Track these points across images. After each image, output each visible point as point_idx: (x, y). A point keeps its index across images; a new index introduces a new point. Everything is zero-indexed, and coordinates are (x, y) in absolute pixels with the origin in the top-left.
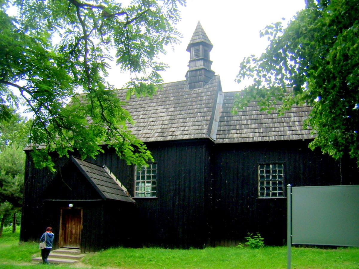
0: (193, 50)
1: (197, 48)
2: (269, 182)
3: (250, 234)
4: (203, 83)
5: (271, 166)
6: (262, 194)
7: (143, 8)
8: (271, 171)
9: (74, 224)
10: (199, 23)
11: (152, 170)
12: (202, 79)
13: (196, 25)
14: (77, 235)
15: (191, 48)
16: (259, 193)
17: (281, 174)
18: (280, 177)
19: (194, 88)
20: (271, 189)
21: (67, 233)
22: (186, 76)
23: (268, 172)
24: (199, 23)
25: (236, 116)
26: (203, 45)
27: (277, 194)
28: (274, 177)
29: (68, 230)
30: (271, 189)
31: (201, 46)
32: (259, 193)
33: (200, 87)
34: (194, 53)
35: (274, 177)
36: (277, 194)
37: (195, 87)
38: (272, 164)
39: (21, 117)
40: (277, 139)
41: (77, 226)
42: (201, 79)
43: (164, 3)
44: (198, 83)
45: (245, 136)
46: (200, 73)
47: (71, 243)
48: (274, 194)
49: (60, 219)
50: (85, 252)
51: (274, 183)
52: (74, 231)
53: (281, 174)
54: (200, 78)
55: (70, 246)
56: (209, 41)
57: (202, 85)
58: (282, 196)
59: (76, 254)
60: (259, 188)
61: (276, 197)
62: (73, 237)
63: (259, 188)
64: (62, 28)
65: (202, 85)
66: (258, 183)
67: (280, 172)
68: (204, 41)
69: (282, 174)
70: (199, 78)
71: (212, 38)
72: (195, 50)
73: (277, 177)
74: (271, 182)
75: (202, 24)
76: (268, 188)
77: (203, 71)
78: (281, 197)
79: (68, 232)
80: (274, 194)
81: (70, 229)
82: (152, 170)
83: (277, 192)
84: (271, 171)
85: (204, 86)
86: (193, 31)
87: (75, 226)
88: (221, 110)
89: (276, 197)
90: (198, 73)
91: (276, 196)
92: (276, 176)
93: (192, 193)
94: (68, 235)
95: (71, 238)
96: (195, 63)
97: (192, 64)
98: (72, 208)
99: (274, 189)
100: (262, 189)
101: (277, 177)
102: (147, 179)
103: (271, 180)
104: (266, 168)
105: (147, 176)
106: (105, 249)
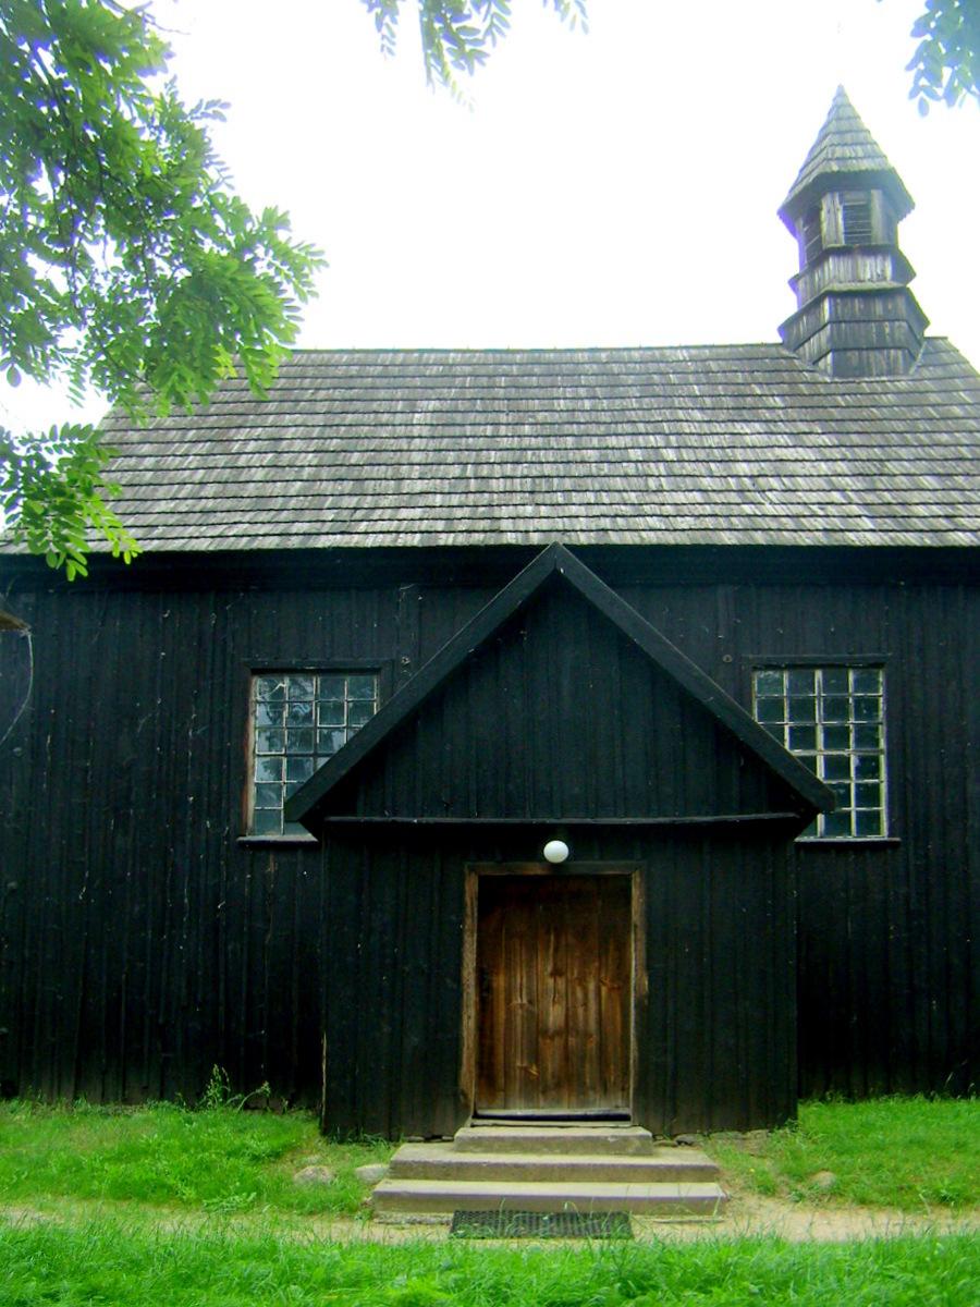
0: (841, 208)
9: (556, 973)
10: (841, 93)
11: (858, 701)
12: (897, 335)
13: (833, 93)
14: (587, 1035)
19: (862, 375)
21: (501, 1029)
22: (785, 329)
24: (841, 93)
29: (509, 1012)
34: (841, 221)
37: (863, 370)
39: (211, 153)
41: (582, 980)
43: (282, 235)
44: (877, 353)
47: (535, 1088)
49: (460, 944)
50: (672, 1137)
52: (554, 1015)
54: (887, 330)
55: (530, 1100)
59: (620, 1146)
62: (552, 1053)
72: (845, 208)
79: (509, 1021)
81: (520, 1000)
82: (858, 701)
87: (561, 982)
90: (878, 308)
93: (200, 949)
94: (522, 1051)
95: (536, 1056)
96: (855, 268)
98: (556, 867)
102: (827, 745)
105: (828, 731)
106: (850, 1098)
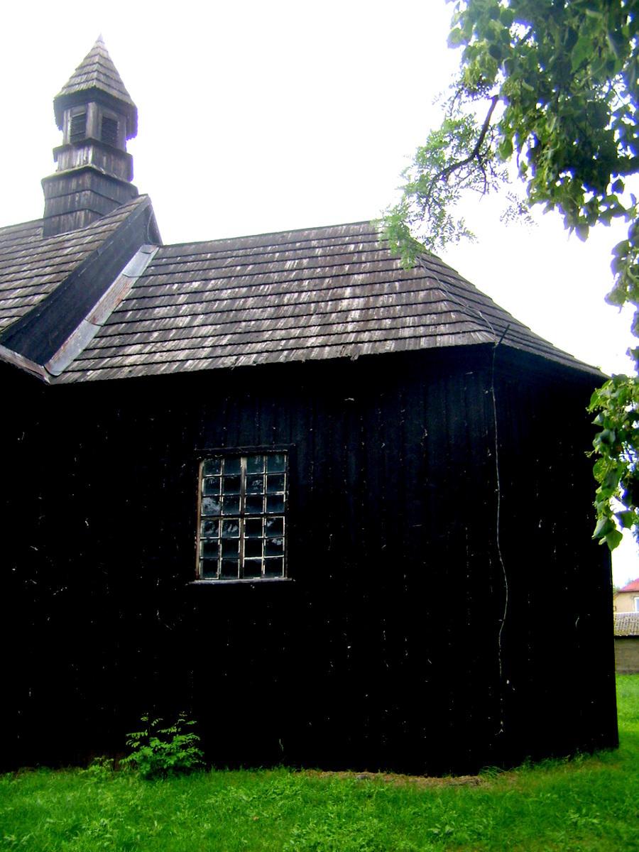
0: (69, 119)
1: (79, 110)
2: (236, 523)
3: (151, 720)
4: (86, 216)
5: (244, 463)
6: (210, 568)
7: (621, 812)
8: (244, 482)
13: (92, 45)
15: (63, 113)
16: (199, 565)
17: (278, 493)
18: (274, 501)
20: (242, 548)
23: (232, 484)
24: (99, 40)
25: (166, 306)
26: (99, 102)
27: (263, 568)
28: (255, 503)
30: (242, 548)
31: (92, 108)
32: (199, 565)
33: (76, 227)
35: (255, 503)
36: (263, 568)
38: (244, 456)
40: (262, 359)
42: (79, 202)
44: (69, 216)
45: (164, 359)
46: (78, 185)
48: (253, 568)
51: (253, 528)
53: (278, 493)
54: (77, 199)
56: (126, 94)
57: (82, 222)
58: (279, 573)
60: (200, 545)
61: (257, 579)
63: (200, 545)
64: (583, 760)
65: (82, 222)
66: (195, 527)
67: (274, 482)
68: (100, 86)
69: (283, 493)
70: (73, 200)
71: (136, 89)
73: (265, 502)
74: (242, 522)
75: (107, 46)
76: (230, 546)
77: (87, 179)
78: (276, 578)
80: (253, 568)
83: (262, 558)
84: (244, 482)
85: (87, 222)
86: (79, 61)
88: (128, 293)
89: (257, 579)
91: (259, 573)
92: (260, 499)
97: (64, 158)
99: (253, 548)
100: (210, 548)
101: (265, 502)
103: (242, 516)
104: (227, 468)
